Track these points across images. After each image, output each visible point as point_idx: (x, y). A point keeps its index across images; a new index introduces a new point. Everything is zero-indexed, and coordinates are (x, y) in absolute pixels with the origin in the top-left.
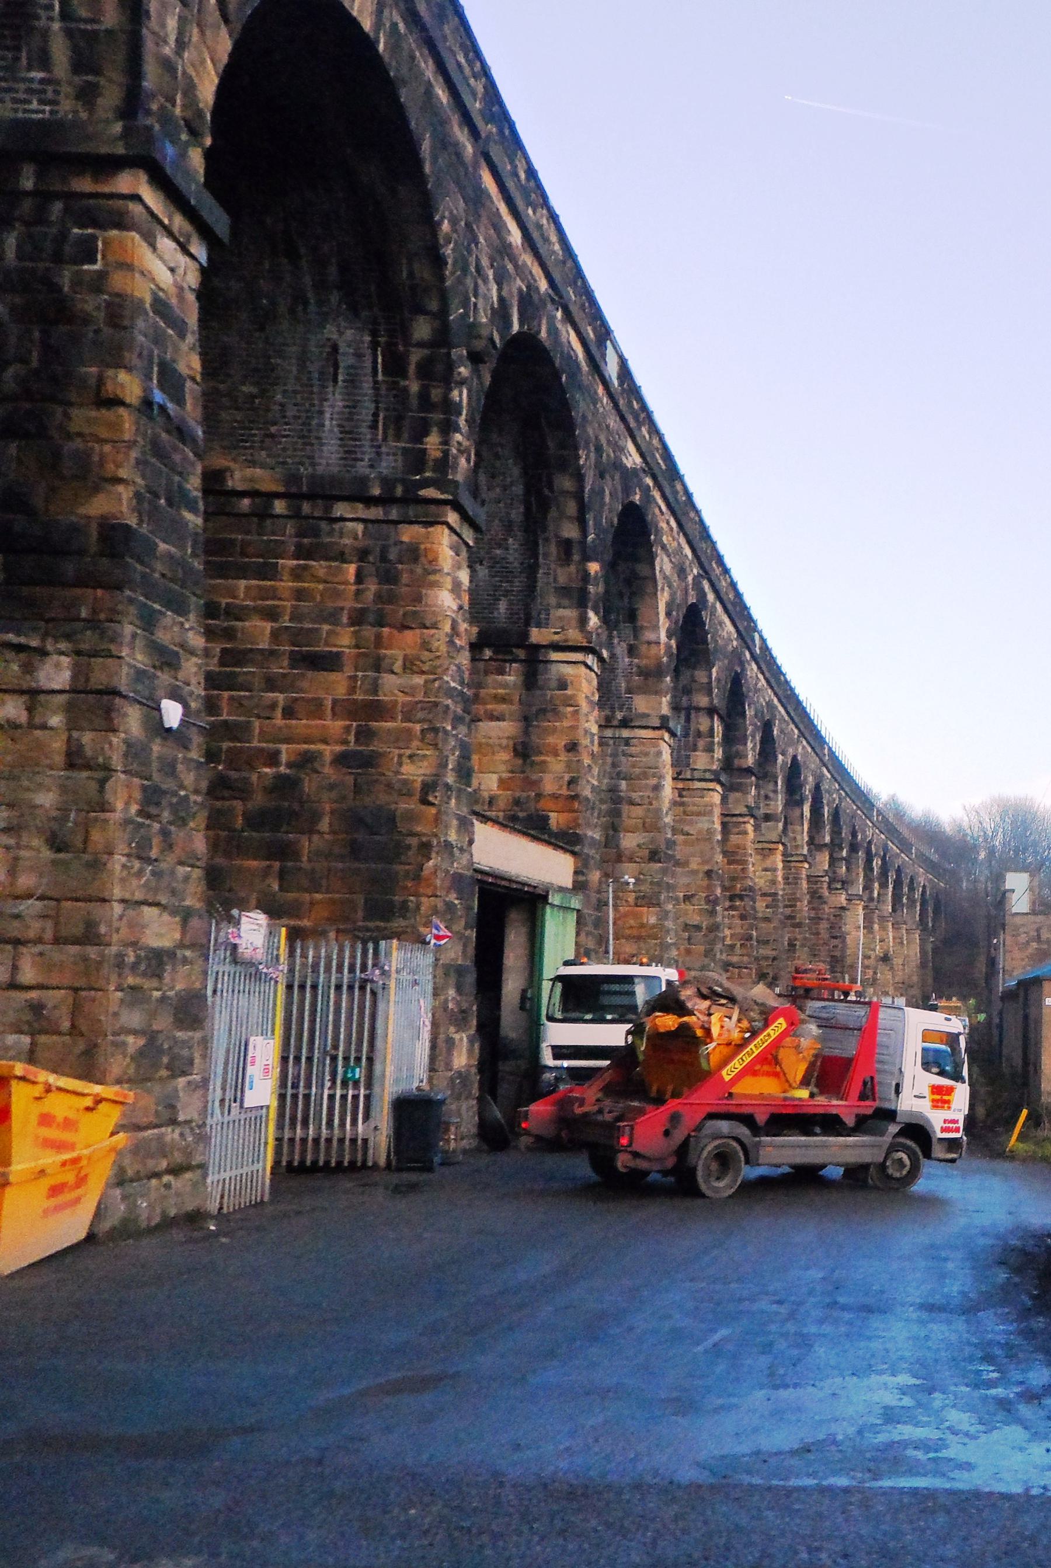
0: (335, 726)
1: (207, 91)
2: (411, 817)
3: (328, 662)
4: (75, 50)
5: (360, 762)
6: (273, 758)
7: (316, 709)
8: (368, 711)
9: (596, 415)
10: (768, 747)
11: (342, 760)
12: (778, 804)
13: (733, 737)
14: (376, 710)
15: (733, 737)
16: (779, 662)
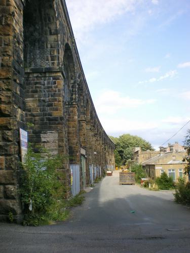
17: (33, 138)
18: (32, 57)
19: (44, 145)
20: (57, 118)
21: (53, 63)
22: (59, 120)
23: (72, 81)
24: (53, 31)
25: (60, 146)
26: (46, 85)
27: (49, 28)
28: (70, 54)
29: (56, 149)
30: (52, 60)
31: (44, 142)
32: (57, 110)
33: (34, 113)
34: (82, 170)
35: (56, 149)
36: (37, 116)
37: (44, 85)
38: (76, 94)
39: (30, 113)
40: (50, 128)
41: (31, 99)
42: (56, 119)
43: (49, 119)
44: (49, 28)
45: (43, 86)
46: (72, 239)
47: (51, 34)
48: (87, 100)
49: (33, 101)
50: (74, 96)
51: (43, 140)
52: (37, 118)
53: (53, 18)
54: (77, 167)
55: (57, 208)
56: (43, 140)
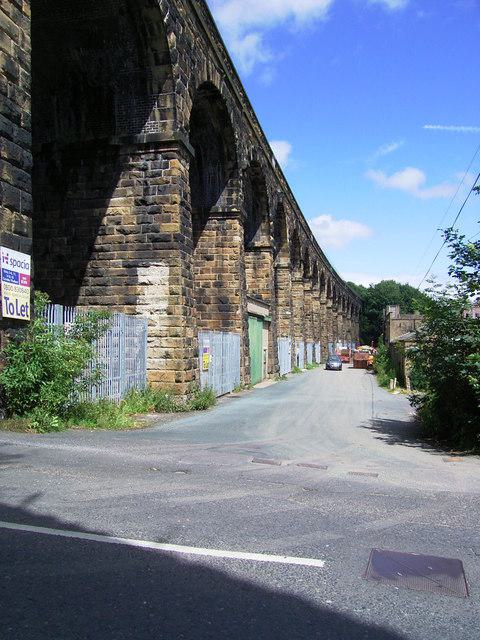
0: (213, 275)
1: (188, 116)
2: (233, 299)
3: (209, 259)
4: (161, 114)
5: (219, 285)
6: (198, 285)
7: (208, 270)
8: (221, 270)
9: (270, 179)
10: (315, 270)
11: (215, 285)
12: (318, 286)
13: (306, 268)
14: (223, 270)
15: (306, 268)
16: (357, 284)
17: (122, 275)
18: (124, 113)
19: (142, 290)
20: (169, 235)
21: (164, 125)
22: (173, 239)
23: (230, 165)
24: (161, 56)
25: (172, 293)
26: (150, 170)
27: (152, 49)
28: (221, 108)
29: (164, 299)
30: (162, 119)
31: (144, 284)
32: (168, 220)
33: (127, 227)
34: (247, 345)
35: (164, 299)
36: (131, 232)
37: (145, 169)
38: (238, 191)
39: (118, 227)
40: (155, 257)
41: (120, 199)
42: (165, 239)
43: (155, 240)
44: (152, 49)
45: (143, 173)
46: (186, 471)
47: (157, 63)
48: (280, 205)
49: (125, 202)
50: (234, 195)
51: (141, 279)
52: (131, 237)
53: (159, 27)
54: (233, 339)
55: (103, 419)
56: (141, 279)
